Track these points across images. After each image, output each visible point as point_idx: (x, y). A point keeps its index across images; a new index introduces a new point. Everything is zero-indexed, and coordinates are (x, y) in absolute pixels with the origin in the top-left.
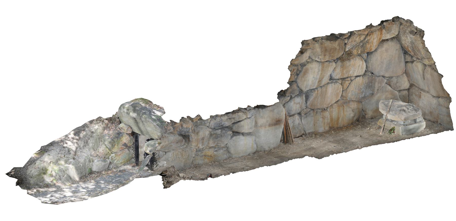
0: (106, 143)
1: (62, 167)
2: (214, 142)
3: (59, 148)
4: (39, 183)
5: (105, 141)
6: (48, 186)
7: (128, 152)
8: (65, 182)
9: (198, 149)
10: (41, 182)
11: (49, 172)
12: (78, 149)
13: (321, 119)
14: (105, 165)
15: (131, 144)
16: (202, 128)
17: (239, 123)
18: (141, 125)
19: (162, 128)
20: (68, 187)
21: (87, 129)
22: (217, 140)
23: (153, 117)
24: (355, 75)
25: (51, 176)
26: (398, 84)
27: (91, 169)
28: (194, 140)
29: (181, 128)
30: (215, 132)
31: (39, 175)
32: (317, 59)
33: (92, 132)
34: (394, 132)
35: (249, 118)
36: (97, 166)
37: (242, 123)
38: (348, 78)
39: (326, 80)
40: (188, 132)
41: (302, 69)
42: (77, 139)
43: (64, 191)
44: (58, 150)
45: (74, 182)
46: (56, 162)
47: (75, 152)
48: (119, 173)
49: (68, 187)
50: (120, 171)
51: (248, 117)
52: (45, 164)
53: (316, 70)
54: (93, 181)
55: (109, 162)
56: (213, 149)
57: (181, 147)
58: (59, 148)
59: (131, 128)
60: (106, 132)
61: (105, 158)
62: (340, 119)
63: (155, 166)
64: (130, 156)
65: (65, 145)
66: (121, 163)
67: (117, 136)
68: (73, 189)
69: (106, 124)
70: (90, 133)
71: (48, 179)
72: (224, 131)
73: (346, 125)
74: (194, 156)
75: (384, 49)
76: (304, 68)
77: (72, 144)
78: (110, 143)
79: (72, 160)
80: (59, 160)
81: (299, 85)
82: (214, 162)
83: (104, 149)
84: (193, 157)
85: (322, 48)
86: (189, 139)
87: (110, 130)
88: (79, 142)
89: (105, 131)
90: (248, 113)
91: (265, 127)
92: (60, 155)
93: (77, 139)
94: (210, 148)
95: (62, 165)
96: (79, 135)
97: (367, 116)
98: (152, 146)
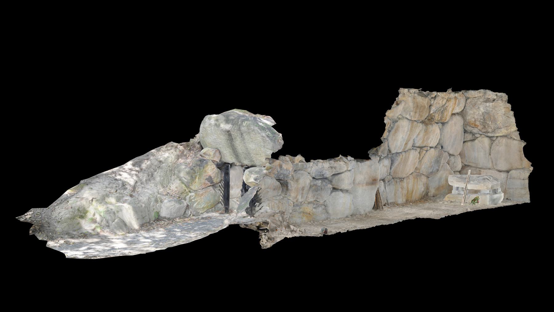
0: (182, 175)
1: (111, 207)
2: (314, 196)
3: (108, 181)
4: (71, 232)
5: (179, 172)
6: (86, 235)
7: (213, 191)
8: (115, 230)
9: (295, 203)
10: (74, 231)
11: (90, 215)
12: (139, 183)
13: (400, 189)
14: (179, 209)
15: (218, 180)
16: (302, 174)
17: (340, 175)
18: (238, 143)
19: (274, 142)
20: (121, 237)
21: (152, 158)
22: (317, 193)
23: (261, 124)
24: (430, 146)
25: (94, 221)
26: (455, 164)
27: (158, 213)
28: (293, 188)
29: (279, 170)
30: (315, 183)
31: (73, 218)
32: (408, 116)
33: (160, 162)
34: (478, 202)
35: (350, 170)
36: (167, 208)
37: (343, 175)
38: (425, 147)
39: (410, 145)
40: (287, 176)
41: (394, 125)
42: (137, 171)
43: (112, 242)
44: (106, 183)
45: (130, 230)
46: (102, 200)
47: (134, 187)
48: (202, 221)
49: (121, 237)
50: (203, 218)
51: (349, 169)
52: (84, 202)
53: (406, 129)
54: (162, 229)
55: (185, 204)
56: (312, 205)
57: (278, 198)
58: (108, 181)
59: (220, 153)
60: (181, 161)
61: (179, 199)
62: (414, 193)
63: (257, 209)
64: (216, 198)
65: (118, 177)
66: (203, 208)
67: (199, 163)
68: (129, 240)
69: (180, 151)
70: (156, 163)
71: (87, 226)
72: (324, 183)
73: (417, 199)
74: (291, 211)
75: (453, 122)
76: (396, 124)
77: (128, 176)
78: (188, 173)
79: (128, 198)
80: (107, 196)
81: (390, 144)
82: (314, 221)
83: (177, 185)
84: (291, 214)
85: (414, 103)
86: (287, 186)
87: (187, 158)
88: (141, 175)
89: (180, 160)
90: (349, 163)
91: (363, 186)
92: (108, 189)
93: (137, 171)
94: (309, 203)
95: (111, 204)
96: (140, 166)
97: (429, 194)
98: (256, 172)
